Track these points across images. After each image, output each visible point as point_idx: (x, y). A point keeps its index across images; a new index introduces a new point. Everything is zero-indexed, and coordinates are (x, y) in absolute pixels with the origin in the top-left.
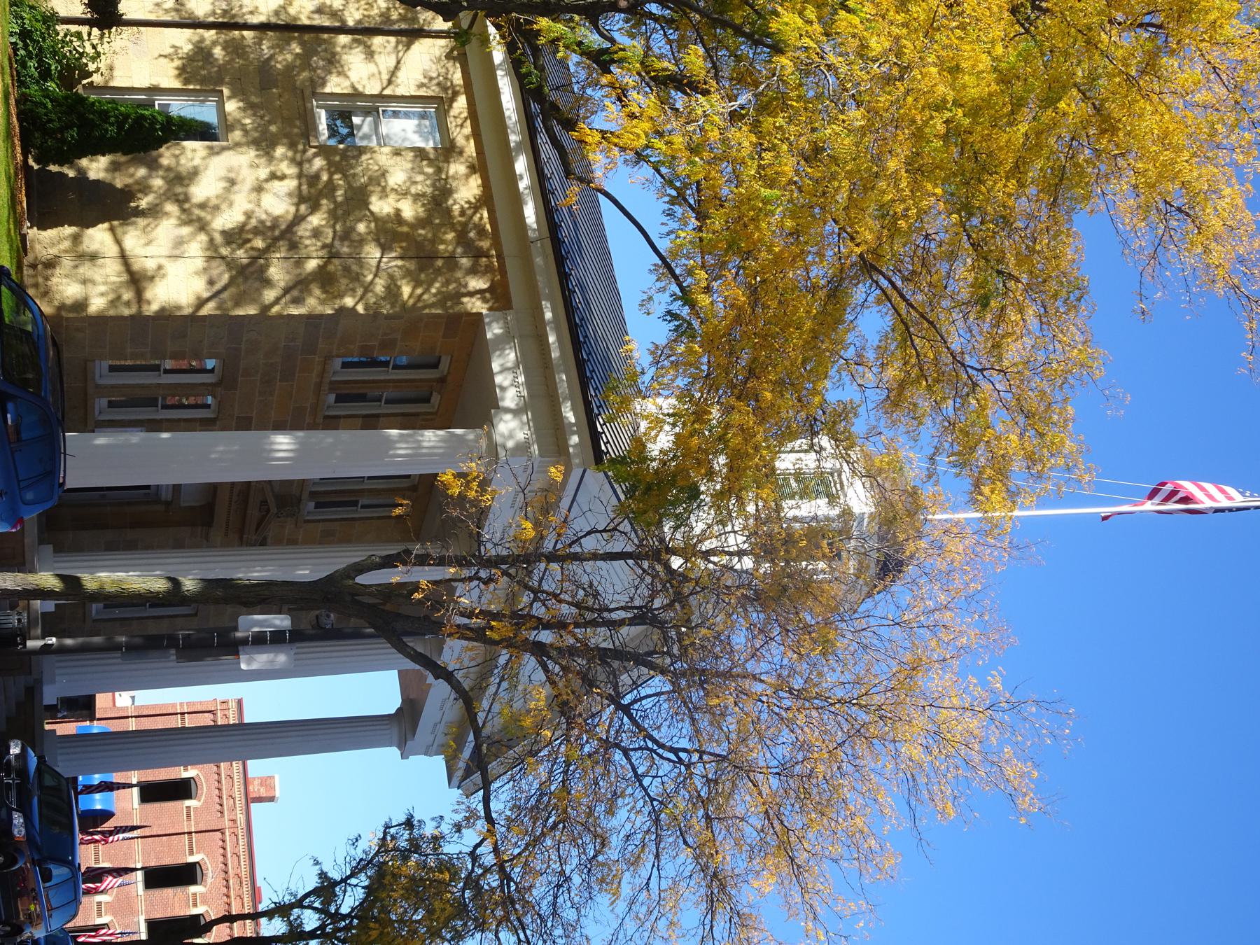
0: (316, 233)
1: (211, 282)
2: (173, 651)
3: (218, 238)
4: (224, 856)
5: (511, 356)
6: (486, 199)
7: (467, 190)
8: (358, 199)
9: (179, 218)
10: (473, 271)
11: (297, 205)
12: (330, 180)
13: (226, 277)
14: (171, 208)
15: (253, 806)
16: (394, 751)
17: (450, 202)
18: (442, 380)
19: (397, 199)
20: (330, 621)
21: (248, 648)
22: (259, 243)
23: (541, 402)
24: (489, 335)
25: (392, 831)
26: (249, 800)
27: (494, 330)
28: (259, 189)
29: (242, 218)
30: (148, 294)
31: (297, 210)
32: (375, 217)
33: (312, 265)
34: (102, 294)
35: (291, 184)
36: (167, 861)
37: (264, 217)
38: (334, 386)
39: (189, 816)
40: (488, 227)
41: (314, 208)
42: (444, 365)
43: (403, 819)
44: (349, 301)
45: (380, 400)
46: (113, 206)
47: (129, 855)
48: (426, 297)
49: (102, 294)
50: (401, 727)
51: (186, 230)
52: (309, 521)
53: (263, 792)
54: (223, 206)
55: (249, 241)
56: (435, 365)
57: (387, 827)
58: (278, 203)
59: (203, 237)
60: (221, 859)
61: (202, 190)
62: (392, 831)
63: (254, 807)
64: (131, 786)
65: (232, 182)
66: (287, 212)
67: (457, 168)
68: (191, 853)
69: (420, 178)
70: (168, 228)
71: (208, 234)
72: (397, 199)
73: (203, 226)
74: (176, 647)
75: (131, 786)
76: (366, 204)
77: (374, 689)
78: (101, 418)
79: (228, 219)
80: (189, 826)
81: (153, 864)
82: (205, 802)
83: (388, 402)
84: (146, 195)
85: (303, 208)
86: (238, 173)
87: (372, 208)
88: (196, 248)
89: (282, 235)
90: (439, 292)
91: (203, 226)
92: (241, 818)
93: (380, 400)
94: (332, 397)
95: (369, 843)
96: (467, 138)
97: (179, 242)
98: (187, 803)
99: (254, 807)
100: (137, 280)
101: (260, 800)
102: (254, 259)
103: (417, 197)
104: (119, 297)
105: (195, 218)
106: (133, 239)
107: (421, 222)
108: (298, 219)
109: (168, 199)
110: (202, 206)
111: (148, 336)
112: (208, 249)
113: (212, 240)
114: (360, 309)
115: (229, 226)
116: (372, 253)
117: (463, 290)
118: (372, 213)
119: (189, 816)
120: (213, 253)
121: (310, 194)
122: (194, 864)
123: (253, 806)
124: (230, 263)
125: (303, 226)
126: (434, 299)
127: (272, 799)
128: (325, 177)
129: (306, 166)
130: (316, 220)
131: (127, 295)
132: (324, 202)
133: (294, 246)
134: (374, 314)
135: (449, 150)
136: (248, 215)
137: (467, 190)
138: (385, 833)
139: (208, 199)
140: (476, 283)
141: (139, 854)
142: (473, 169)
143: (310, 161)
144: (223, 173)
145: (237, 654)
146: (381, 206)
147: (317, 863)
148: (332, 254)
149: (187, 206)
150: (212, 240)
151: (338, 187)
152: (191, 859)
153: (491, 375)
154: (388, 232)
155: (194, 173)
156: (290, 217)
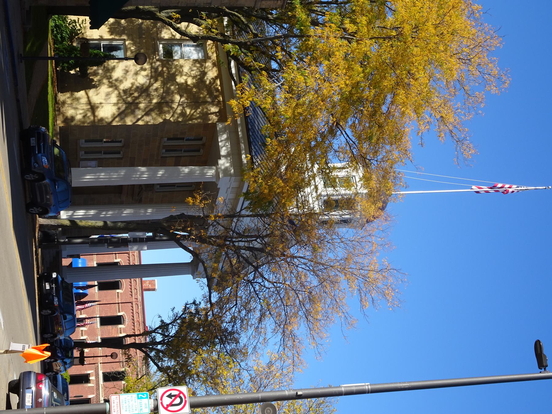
0: (156, 90)
1: (119, 109)
2: (106, 244)
3: (121, 91)
4: (133, 313)
5: (225, 136)
6: (219, 76)
7: (212, 74)
8: (172, 78)
9: (108, 85)
10: (212, 103)
11: (150, 79)
12: (162, 70)
13: (124, 106)
14: (105, 81)
15: (145, 292)
16: (190, 276)
17: (205, 78)
18: (203, 145)
19: (186, 76)
20: (162, 233)
21: (131, 244)
22: (136, 94)
23: (235, 155)
24: (218, 129)
25: (188, 306)
26: (143, 290)
27: (220, 126)
28: (136, 74)
29: (130, 85)
30: (97, 114)
31: (150, 82)
32: (178, 84)
33: (155, 101)
34: (80, 114)
35: (147, 72)
36: (109, 314)
37: (138, 85)
38: (164, 147)
39: (118, 296)
40: (220, 88)
41: (156, 81)
42: (204, 139)
43: (192, 302)
44: (168, 117)
45: (181, 151)
46: (85, 83)
47: (94, 312)
48: (195, 114)
49: (80, 114)
50: (190, 269)
51: (111, 89)
52: (156, 192)
53: (150, 287)
54: (124, 81)
55: (133, 94)
56: (201, 139)
57: (186, 304)
58: (142, 80)
59: (116, 92)
60: (131, 314)
61: (117, 74)
62: (188, 306)
63: (145, 293)
64: (95, 286)
65: (127, 71)
66: (146, 82)
67: (209, 64)
68: (119, 312)
69: (195, 68)
70: (104, 89)
71: (118, 91)
72: (186, 76)
73: (116, 88)
74: (107, 243)
75: (95, 286)
76: (175, 80)
77: (179, 255)
78: (82, 157)
79: (126, 85)
80: (118, 300)
81: (103, 315)
82: (125, 290)
83: (185, 151)
84: (97, 76)
85: (152, 80)
86: (129, 68)
87: (177, 80)
88: (114, 98)
89: (144, 90)
90: (200, 112)
91: (116, 88)
92: (140, 298)
93: (181, 151)
94: (164, 151)
95: (179, 310)
96: (213, 53)
97: (108, 95)
98: (118, 291)
99: (145, 293)
100: (93, 108)
101: (149, 290)
102: (134, 101)
103: (194, 77)
104: (86, 115)
105: (113, 85)
106: (92, 92)
107: (195, 85)
108: (151, 85)
109: (104, 78)
110: (116, 80)
111: (97, 129)
112: (43, 342)
113: (119, 93)
114: (171, 119)
115: (126, 88)
116: (177, 98)
117: (209, 112)
118: (177, 82)
119: (118, 296)
120: (119, 96)
121: (155, 75)
122: (120, 316)
123: (145, 292)
124: (125, 102)
125: (151, 88)
126: (198, 115)
127: (154, 290)
128: (160, 69)
129: (153, 64)
130: (157, 85)
131: (89, 114)
132: (159, 78)
133: (149, 95)
134: (177, 122)
135: (207, 57)
136: (133, 84)
137: (212, 74)
138: (186, 307)
139: (118, 78)
140: (214, 109)
141: (98, 312)
142: (214, 65)
143: (155, 63)
144: (124, 68)
145: (127, 246)
146: (180, 80)
147: (160, 317)
148: (162, 98)
149: (111, 80)
150: (119, 93)
151: (166, 73)
152: (119, 314)
153: (218, 142)
154: (184, 89)
155: (114, 68)
156: (147, 84)
